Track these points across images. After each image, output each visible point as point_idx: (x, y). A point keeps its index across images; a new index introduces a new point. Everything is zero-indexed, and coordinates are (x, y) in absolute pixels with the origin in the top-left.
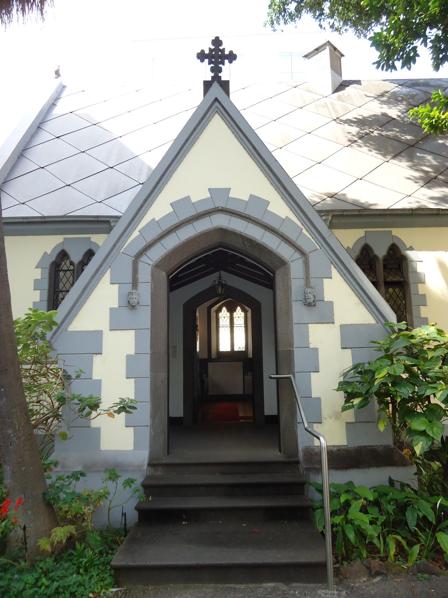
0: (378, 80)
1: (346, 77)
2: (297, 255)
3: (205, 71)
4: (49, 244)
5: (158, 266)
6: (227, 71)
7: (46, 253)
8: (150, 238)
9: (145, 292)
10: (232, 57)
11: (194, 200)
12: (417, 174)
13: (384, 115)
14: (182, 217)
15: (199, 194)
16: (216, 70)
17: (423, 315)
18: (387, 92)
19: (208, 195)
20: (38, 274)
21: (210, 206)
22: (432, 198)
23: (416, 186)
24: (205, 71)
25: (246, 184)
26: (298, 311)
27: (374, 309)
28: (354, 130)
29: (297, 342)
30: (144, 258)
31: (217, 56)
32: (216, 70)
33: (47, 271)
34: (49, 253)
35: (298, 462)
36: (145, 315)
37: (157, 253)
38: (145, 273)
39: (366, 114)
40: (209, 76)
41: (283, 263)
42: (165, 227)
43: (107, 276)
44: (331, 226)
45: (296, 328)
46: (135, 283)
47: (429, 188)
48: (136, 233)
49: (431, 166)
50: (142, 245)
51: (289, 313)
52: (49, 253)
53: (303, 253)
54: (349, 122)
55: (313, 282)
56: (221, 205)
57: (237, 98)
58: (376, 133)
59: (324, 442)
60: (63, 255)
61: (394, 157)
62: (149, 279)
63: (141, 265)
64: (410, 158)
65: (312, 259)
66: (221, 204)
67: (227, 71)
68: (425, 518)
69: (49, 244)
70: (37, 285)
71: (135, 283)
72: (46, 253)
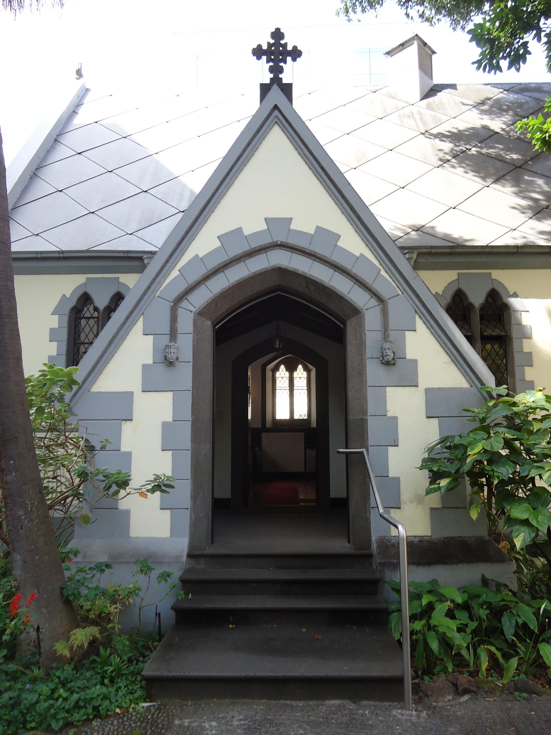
0: (478, 84)
1: (437, 80)
2: (374, 302)
3: (262, 71)
4: (68, 285)
5: (201, 313)
6: (290, 72)
8: (192, 279)
9: (185, 346)
10: (296, 54)
11: (246, 232)
12: (524, 203)
13: (485, 128)
15: (253, 225)
16: (276, 70)
18: (489, 99)
19: (264, 227)
20: (54, 322)
21: (266, 241)
22: (542, 233)
24: (262, 71)
25: (312, 213)
26: (373, 371)
28: (447, 146)
29: (371, 409)
30: (184, 304)
31: (277, 52)
32: (276, 70)
33: (66, 319)
36: (185, 374)
37: (201, 297)
39: (462, 126)
40: (267, 78)
41: (355, 311)
43: (139, 326)
45: (370, 391)
46: (173, 334)
47: (539, 220)
48: (175, 273)
49: (542, 193)
51: (362, 372)
54: (441, 136)
55: (392, 335)
57: (302, 105)
58: (474, 151)
60: (85, 299)
61: (496, 181)
62: (190, 329)
63: (180, 312)
64: (517, 182)
65: (392, 306)
66: (280, 238)
67: (290, 72)
69: (68, 285)
70: (53, 335)
71: (173, 334)
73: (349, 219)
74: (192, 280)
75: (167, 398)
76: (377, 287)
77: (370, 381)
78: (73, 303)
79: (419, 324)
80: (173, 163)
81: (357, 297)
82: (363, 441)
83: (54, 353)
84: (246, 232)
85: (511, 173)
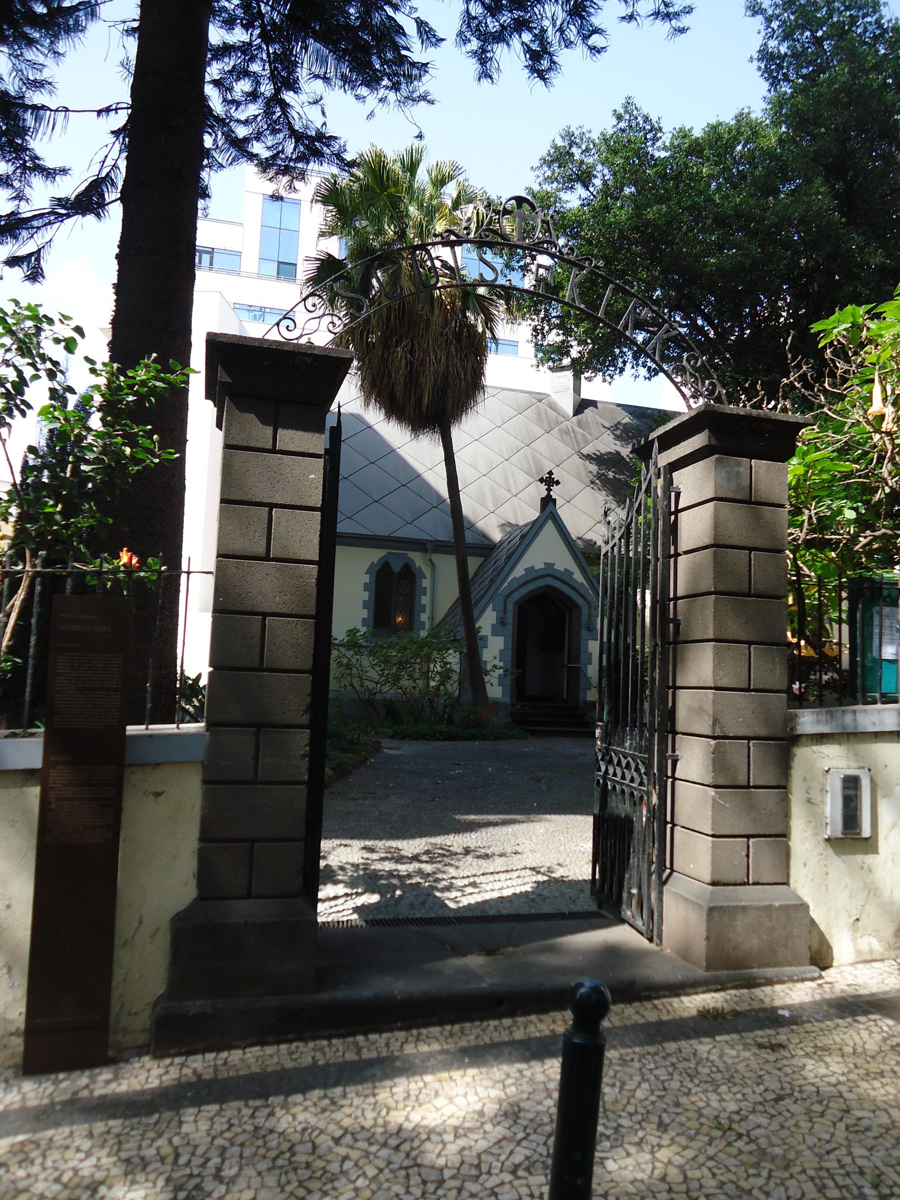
0: (612, 404)
1: (585, 395)
4: (375, 555)
5: (516, 603)
6: (556, 492)
8: (514, 587)
9: (510, 617)
10: (558, 483)
15: (539, 566)
16: (549, 490)
20: (367, 578)
23: (512, 51)
25: (564, 562)
26: (584, 632)
28: (594, 468)
31: (549, 481)
32: (549, 490)
36: (509, 629)
37: (517, 596)
38: (510, 607)
41: (578, 607)
43: (490, 607)
46: (505, 611)
54: (588, 457)
56: (549, 571)
57: (564, 512)
58: (611, 475)
67: (556, 492)
68: (868, 312)
69: (375, 555)
71: (505, 611)
75: (501, 640)
77: (583, 637)
80: (711, 697)
82: (578, 662)
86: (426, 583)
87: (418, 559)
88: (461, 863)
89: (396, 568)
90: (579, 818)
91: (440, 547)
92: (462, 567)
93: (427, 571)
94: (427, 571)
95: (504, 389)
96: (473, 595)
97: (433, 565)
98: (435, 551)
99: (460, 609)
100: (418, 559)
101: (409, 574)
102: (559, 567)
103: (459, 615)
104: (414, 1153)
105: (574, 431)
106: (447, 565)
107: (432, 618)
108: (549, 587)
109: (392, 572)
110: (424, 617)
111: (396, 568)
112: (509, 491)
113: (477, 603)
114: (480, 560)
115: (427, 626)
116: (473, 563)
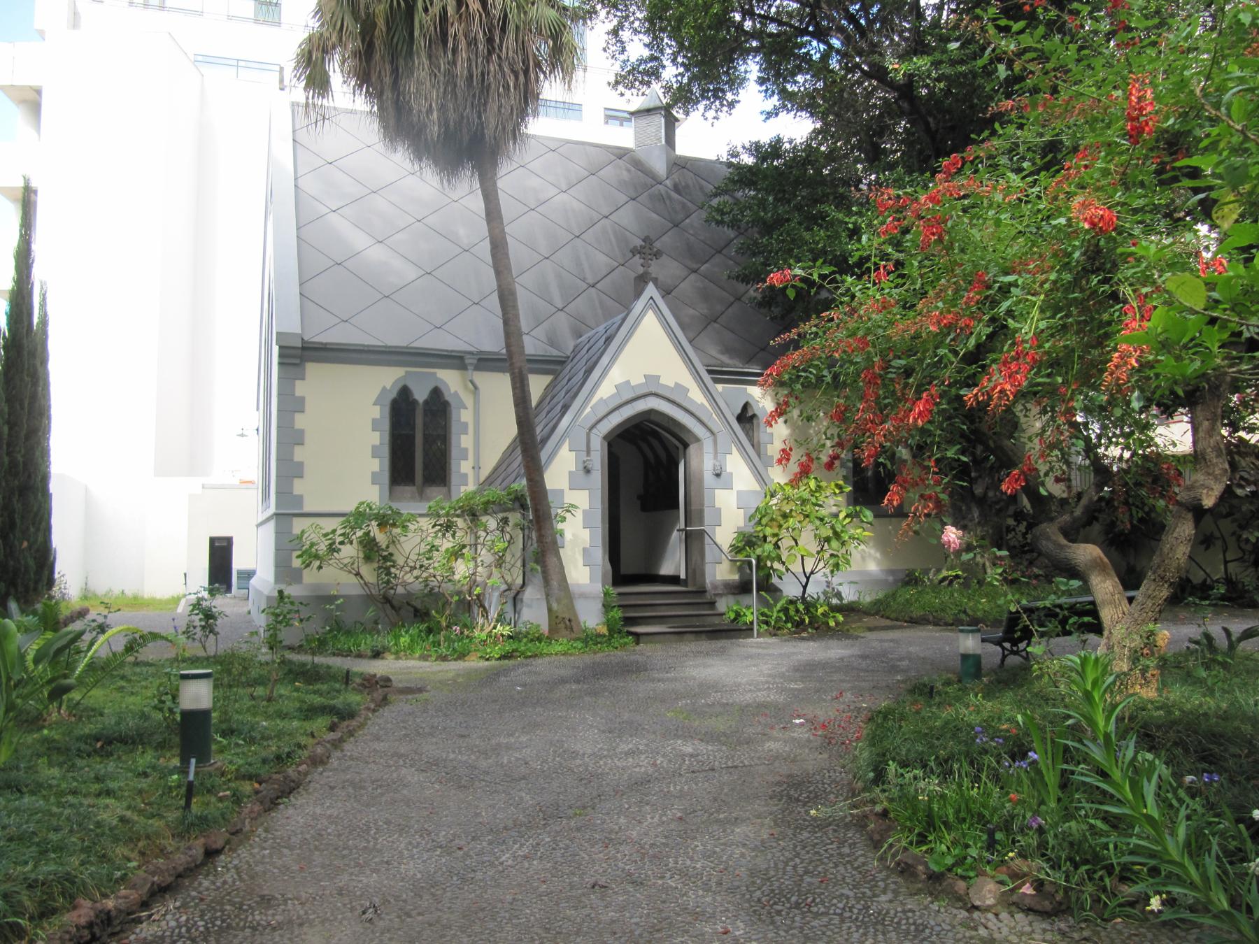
2: (708, 434)
7: (384, 388)
11: (633, 384)
14: (625, 398)
15: (637, 380)
17: (377, 461)
20: (376, 412)
21: (645, 391)
27: (372, 357)
29: (706, 504)
30: (594, 431)
33: (387, 410)
34: (388, 387)
35: (705, 592)
42: (612, 406)
43: (566, 446)
44: (716, 381)
48: (588, 409)
50: (594, 421)
52: (388, 387)
53: (712, 433)
59: (719, 577)
60: (405, 392)
62: (599, 447)
63: (592, 436)
66: (654, 390)
69: (388, 378)
70: (375, 425)
72: (384, 388)
73: (695, 378)
74: (600, 415)
76: (709, 424)
78: (394, 395)
79: (734, 449)
81: (641, 406)
82: (701, 522)
83: (377, 442)
84: (633, 384)
85: (644, 121)
86: (466, 416)
87: (450, 380)
88: (1187, 644)
89: (421, 395)
90: (500, 375)
91: (486, 362)
92: (521, 399)
93: (468, 399)
94: (468, 399)
95: (568, 142)
96: (538, 430)
97: (476, 388)
98: (478, 368)
99: (519, 451)
100: (450, 380)
101: (439, 406)
102: (668, 380)
103: (518, 458)
104: (1067, 39)
105: (669, 197)
106: (498, 387)
107: (477, 468)
108: (651, 412)
109: (415, 402)
110: (465, 467)
111: (421, 395)
112: (584, 280)
113: (545, 440)
114: (547, 379)
115: (471, 480)
116: (537, 385)
